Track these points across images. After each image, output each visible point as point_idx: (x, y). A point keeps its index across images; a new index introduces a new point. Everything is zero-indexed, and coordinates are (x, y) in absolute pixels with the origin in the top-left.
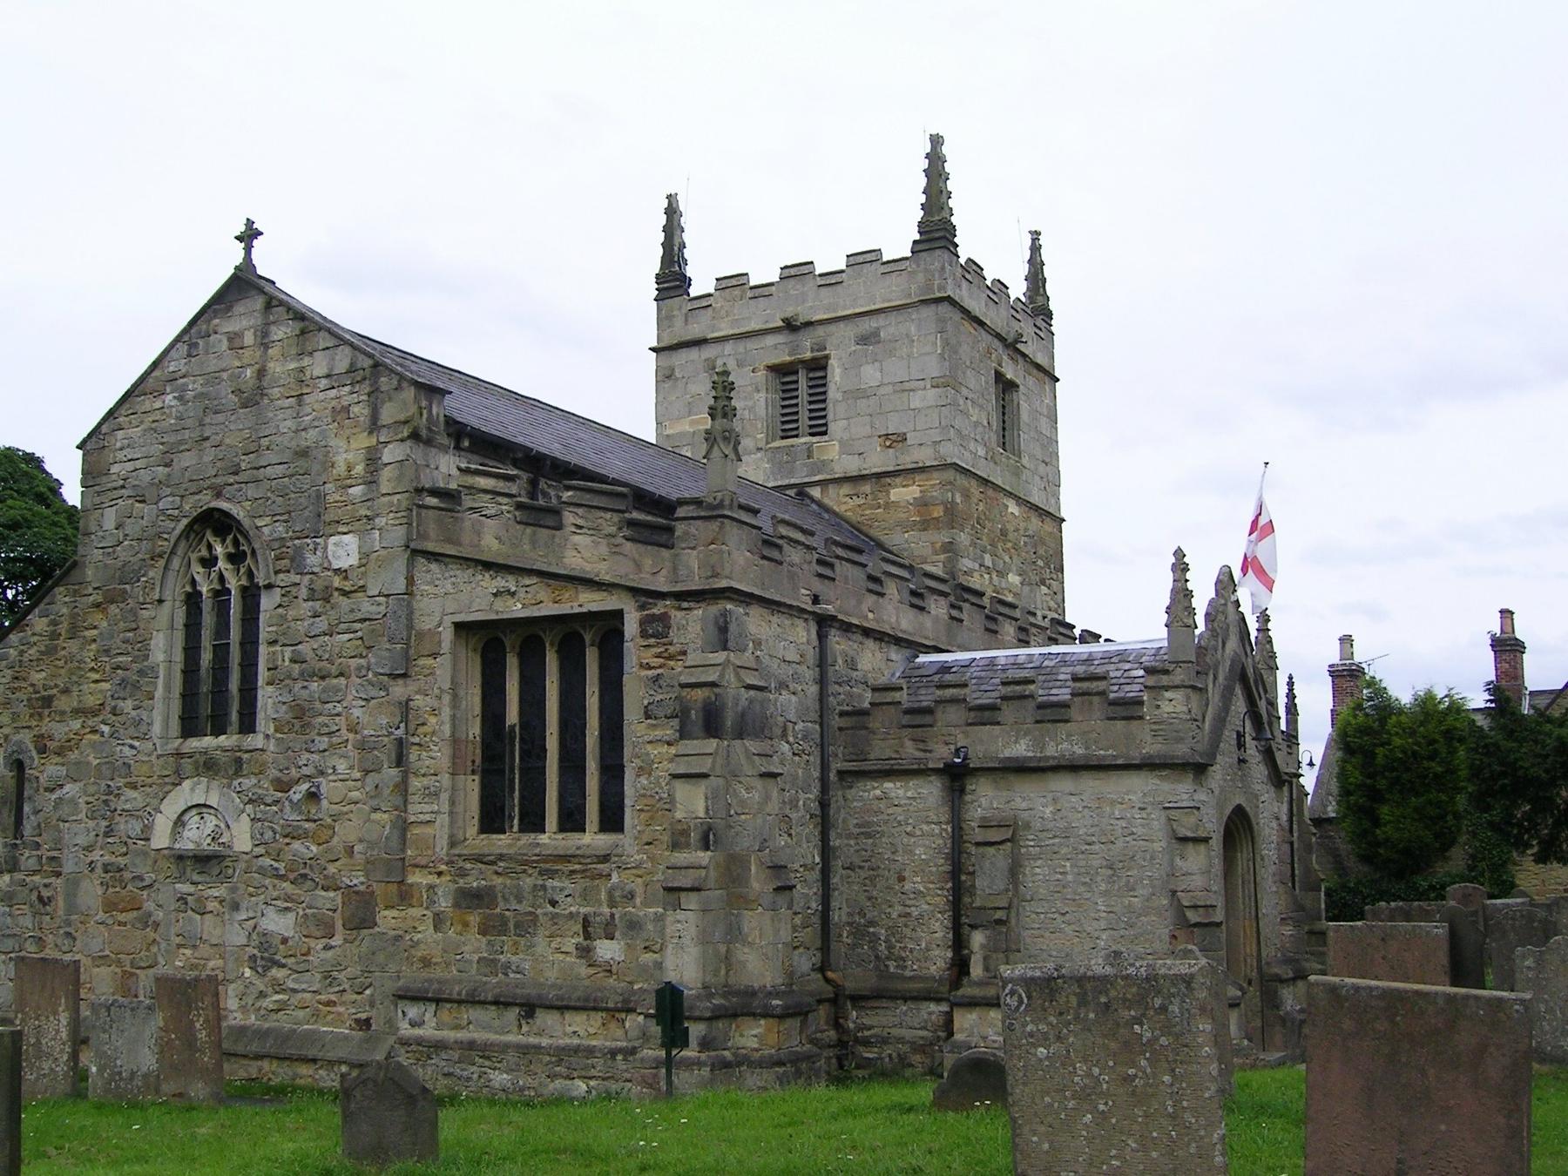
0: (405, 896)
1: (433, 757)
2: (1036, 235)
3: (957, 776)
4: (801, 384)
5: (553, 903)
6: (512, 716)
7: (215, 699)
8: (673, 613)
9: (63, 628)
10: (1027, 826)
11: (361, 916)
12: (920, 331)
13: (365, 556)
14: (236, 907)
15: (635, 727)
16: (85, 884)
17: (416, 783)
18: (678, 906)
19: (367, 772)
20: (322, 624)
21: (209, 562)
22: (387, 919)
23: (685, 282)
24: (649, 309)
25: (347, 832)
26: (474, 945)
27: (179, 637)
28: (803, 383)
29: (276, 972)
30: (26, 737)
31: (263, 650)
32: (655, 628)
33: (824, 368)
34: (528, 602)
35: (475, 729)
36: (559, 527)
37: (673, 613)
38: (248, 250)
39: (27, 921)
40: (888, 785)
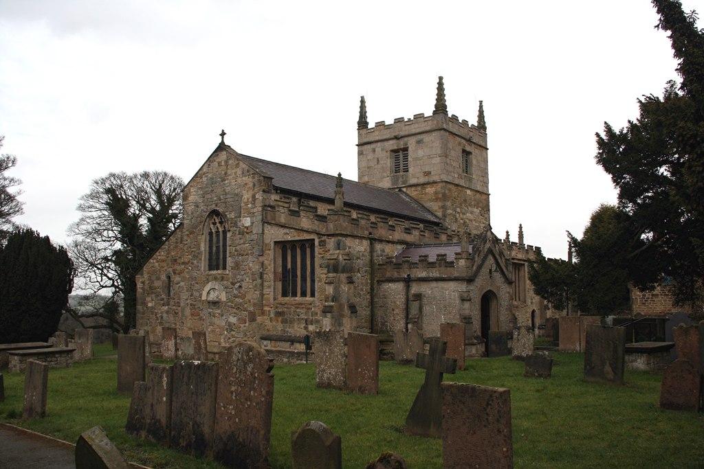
0: (263, 313)
1: (269, 276)
2: (481, 102)
3: (408, 281)
4: (400, 154)
5: (299, 316)
6: (289, 266)
7: (216, 261)
8: (327, 240)
9: (179, 240)
10: (424, 296)
11: (253, 319)
12: (434, 140)
13: (252, 223)
14: (222, 316)
15: (318, 271)
16: (186, 309)
17: (266, 284)
18: (326, 317)
19: (253, 281)
20: (242, 241)
21: (214, 224)
22: (259, 319)
23: (367, 123)
24: (356, 133)
25: (248, 297)
26: (280, 327)
27: (208, 243)
28: (401, 156)
29: (234, 333)
30: (171, 270)
31: (228, 248)
32: (323, 244)
33: (407, 150)
34: (291, 236)
35: (280, 270)
36: (299, 216)
37: (327, 240)
38: (223, 138)
39: (172, 319)
40: (390, 284)
